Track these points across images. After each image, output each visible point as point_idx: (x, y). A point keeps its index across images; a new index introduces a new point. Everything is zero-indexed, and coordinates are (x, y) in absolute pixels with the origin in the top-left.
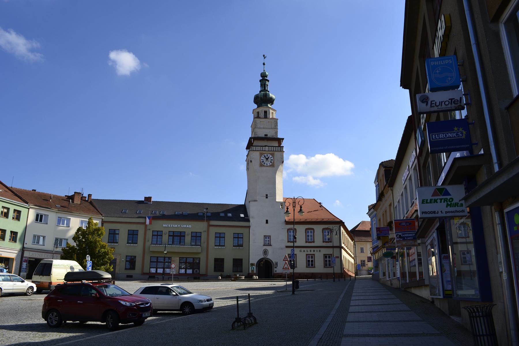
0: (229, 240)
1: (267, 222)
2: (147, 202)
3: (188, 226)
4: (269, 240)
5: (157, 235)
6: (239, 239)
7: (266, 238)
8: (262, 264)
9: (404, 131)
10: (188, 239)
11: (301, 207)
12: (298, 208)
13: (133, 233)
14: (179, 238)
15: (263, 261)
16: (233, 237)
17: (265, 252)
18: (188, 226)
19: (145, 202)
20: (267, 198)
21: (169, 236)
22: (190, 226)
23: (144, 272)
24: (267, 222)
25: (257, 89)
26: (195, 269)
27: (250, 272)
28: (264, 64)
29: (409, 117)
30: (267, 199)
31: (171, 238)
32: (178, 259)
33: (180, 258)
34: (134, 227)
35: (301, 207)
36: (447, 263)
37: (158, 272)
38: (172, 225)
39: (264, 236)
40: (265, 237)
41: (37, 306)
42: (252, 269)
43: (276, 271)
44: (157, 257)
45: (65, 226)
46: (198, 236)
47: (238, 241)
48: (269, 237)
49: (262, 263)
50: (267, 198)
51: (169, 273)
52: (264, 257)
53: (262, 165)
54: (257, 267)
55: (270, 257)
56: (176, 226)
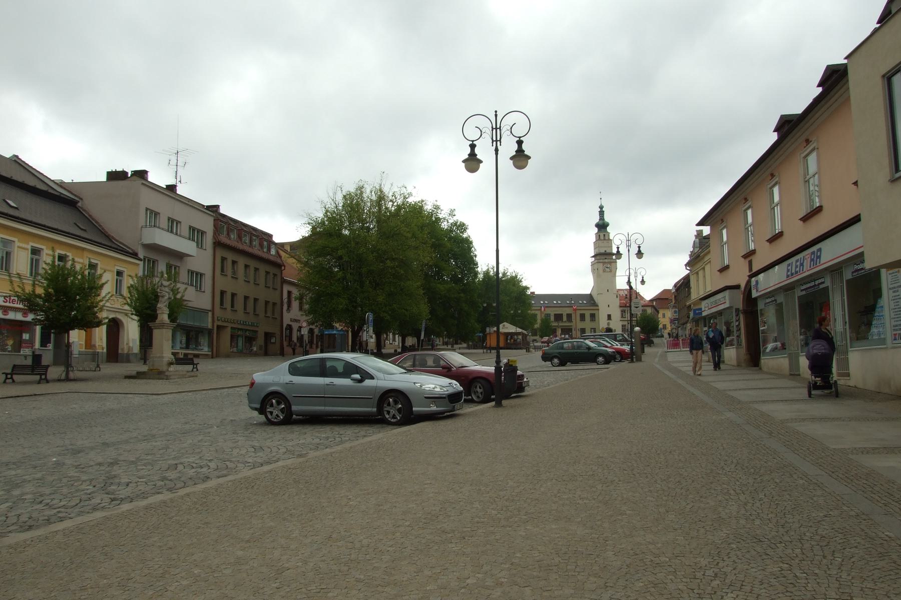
0: (588, 317)
9: (742, 177)
10: (565, 318)
11: (520, 143)
12: (509, 148)
17: (608, 324)
25: (597, 219)
28: (601, 199)
29: (664, 290)
35: (520, 143)
44: (71, 380)
53: (604, 271)
55: (611, 326)
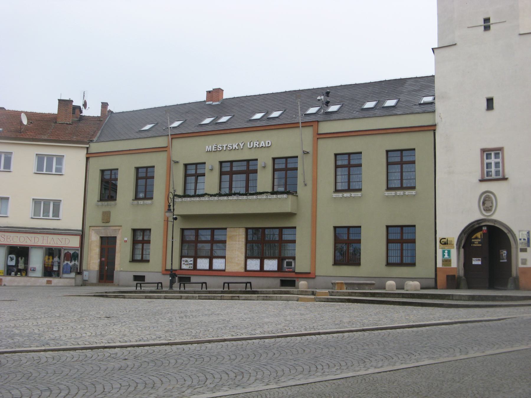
1: (490, 102)
3: (262, 144)
4: (499, 160)
5: (286, 169)
7: (488, 156)
8: (476, 238)
14: (244, 176)
15: (480, 229)
19: (207, 103)
20: (487, 28)
23: (166, 269)
24: (490, 102)
26: (285, 259)
27: (440, 265)
30: (487, 33)
33: (247, 229)
34: (144, 161)
36: (273, 231)
37: (266, 268)
39: (483, 151)
40: (486, 152)
41: (487, 376)
42: (444, 255)
43: (524, 261)
45: (54, 172)
47: (402, 172)
48: (498, 151)
49: (479, 235)
50: (487, 28)
51: (224, 270)
52: (482, 217)
54: (462, 250)
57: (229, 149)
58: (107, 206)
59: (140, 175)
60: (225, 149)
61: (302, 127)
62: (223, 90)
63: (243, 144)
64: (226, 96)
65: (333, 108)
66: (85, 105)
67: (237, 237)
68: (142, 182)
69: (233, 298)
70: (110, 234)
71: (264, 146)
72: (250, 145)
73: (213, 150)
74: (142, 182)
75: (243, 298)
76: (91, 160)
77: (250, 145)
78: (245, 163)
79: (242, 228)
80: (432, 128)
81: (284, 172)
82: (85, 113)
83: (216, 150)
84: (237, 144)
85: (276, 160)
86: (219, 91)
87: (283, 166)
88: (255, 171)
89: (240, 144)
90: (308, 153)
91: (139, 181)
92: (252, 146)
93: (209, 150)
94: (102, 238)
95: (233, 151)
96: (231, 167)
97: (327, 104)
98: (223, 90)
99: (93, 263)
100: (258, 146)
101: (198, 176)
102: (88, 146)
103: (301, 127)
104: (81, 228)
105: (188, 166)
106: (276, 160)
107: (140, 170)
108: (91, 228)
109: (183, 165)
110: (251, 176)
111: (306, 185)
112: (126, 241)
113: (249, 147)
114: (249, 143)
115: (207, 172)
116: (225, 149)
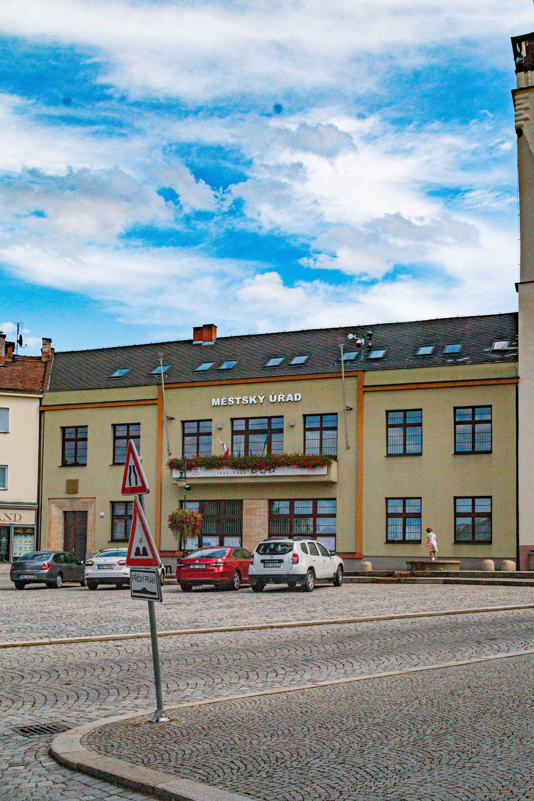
2: (202, 342)
3: (290, 397)
6: (408, 429)
13: (198, 430)
16: (493, 421)
18: (290, 395)
19: (195, 343)
21: (234, 433)
22: (298, 396)
31: (241, 438)
32: (264, 505)
38: (238, 399)
44: (312, 499)
46: (72, 440)
56: (252, 399)
57: (243, 403)
58: (73, 473)
59: (67, 436)
60: (238, 403)
61: (345, 377)
62: (216, 327)
63: (263, 397)
64: (220, 334)
65: (375, 354)
66: (20, 342)
67: (258, 511)
68: (70, 445)
69: (406, 582)
70: (78, 507)
71: (292, 400)
72: (273, 399)
73: (222, 404)
74: (70, 445)
75: (370, 581)
76: (47, 415)
77: (273, 399)
78: (266, 421)
79: (264, 500)
80: (515, 381)
81: (74, 443)
82: (20, 351)
83: (226, 404)
84: (255, 397)
85: (307, 417)
86: (210, 328)
87: (195, 431)
88: (281, 431)
89: (259, 397)
90: (351, 409)
91: (67, 443)
92: (275, 400)
93: (216, 405)
94: (65, 513)
95: (249, 406)
96: (247, 425)
97: (370, 349)
98: (216, 327)
99: (55, 544)
100: (283, 400)
101: (248, 434)
102: (42, 396)
103: (343, 377)
104: (35, 501)
105: (117, 427)
106: (186, 424)
107: (67, 430)
108: (50, 500)
109: (59, 428)
110: (275, 437)
111: (348, 448)
112: (102, 517)
113: (271, 400)
114: (271, 397)
115: (213, 430)
116: (238, 403)
